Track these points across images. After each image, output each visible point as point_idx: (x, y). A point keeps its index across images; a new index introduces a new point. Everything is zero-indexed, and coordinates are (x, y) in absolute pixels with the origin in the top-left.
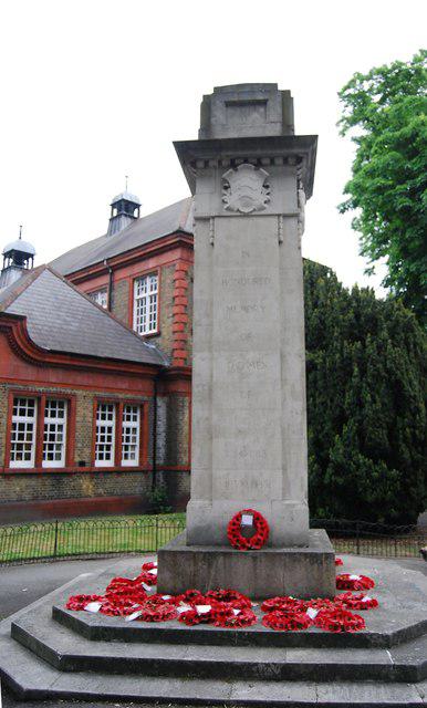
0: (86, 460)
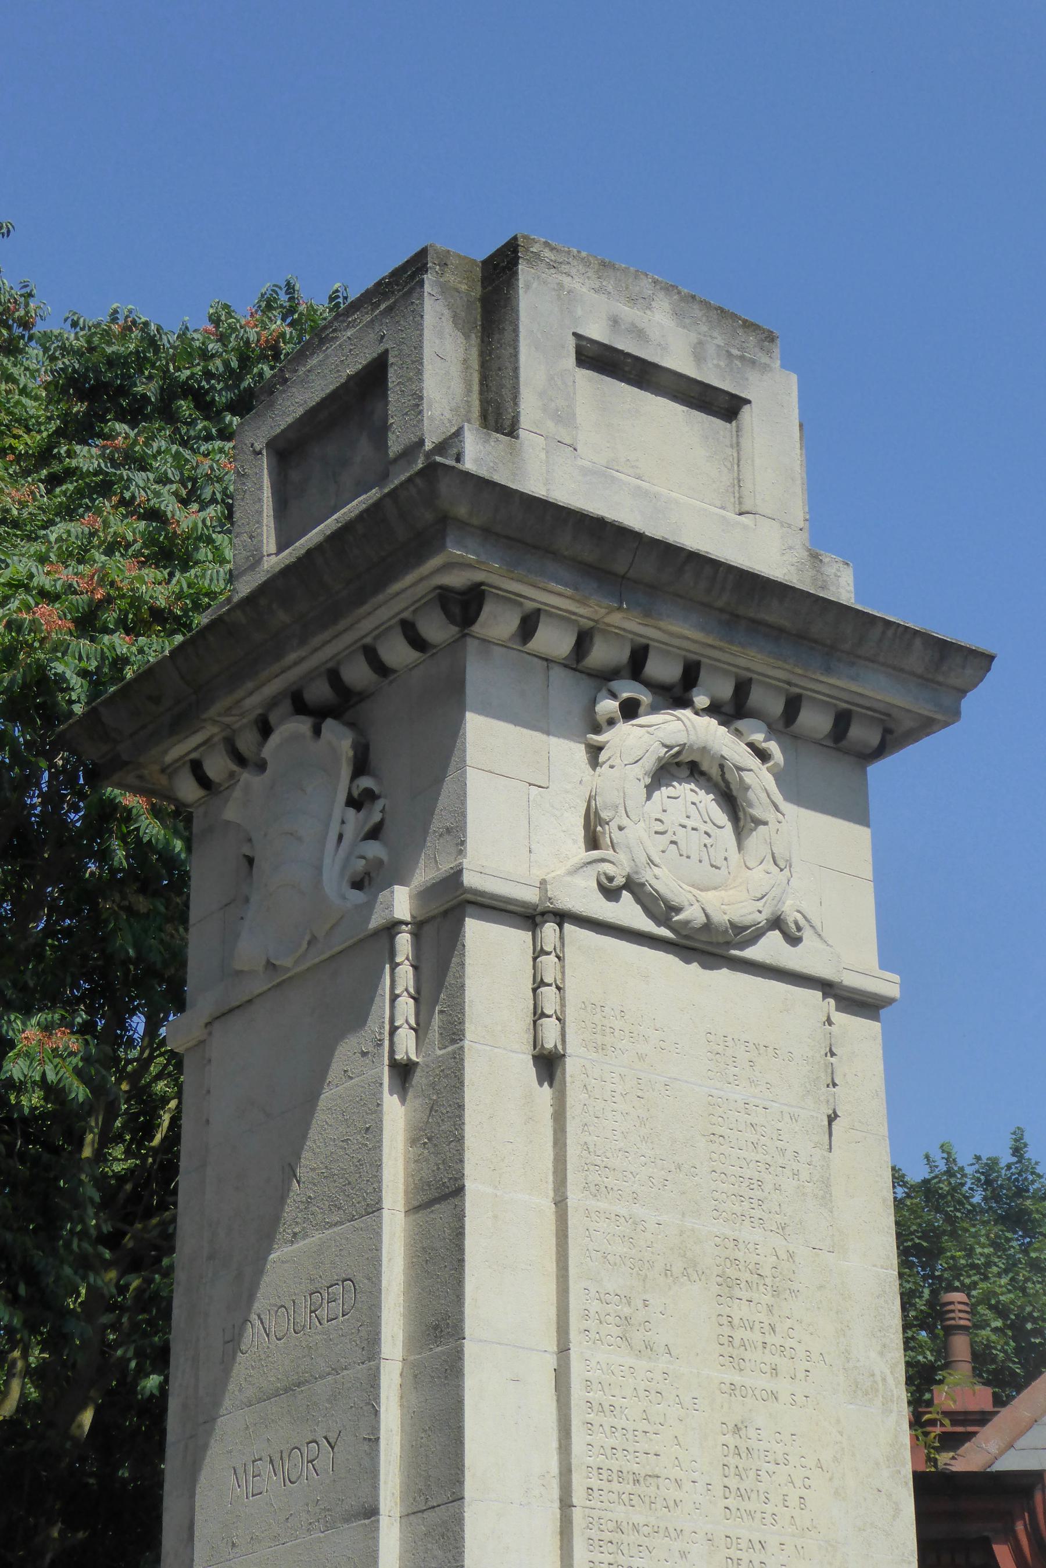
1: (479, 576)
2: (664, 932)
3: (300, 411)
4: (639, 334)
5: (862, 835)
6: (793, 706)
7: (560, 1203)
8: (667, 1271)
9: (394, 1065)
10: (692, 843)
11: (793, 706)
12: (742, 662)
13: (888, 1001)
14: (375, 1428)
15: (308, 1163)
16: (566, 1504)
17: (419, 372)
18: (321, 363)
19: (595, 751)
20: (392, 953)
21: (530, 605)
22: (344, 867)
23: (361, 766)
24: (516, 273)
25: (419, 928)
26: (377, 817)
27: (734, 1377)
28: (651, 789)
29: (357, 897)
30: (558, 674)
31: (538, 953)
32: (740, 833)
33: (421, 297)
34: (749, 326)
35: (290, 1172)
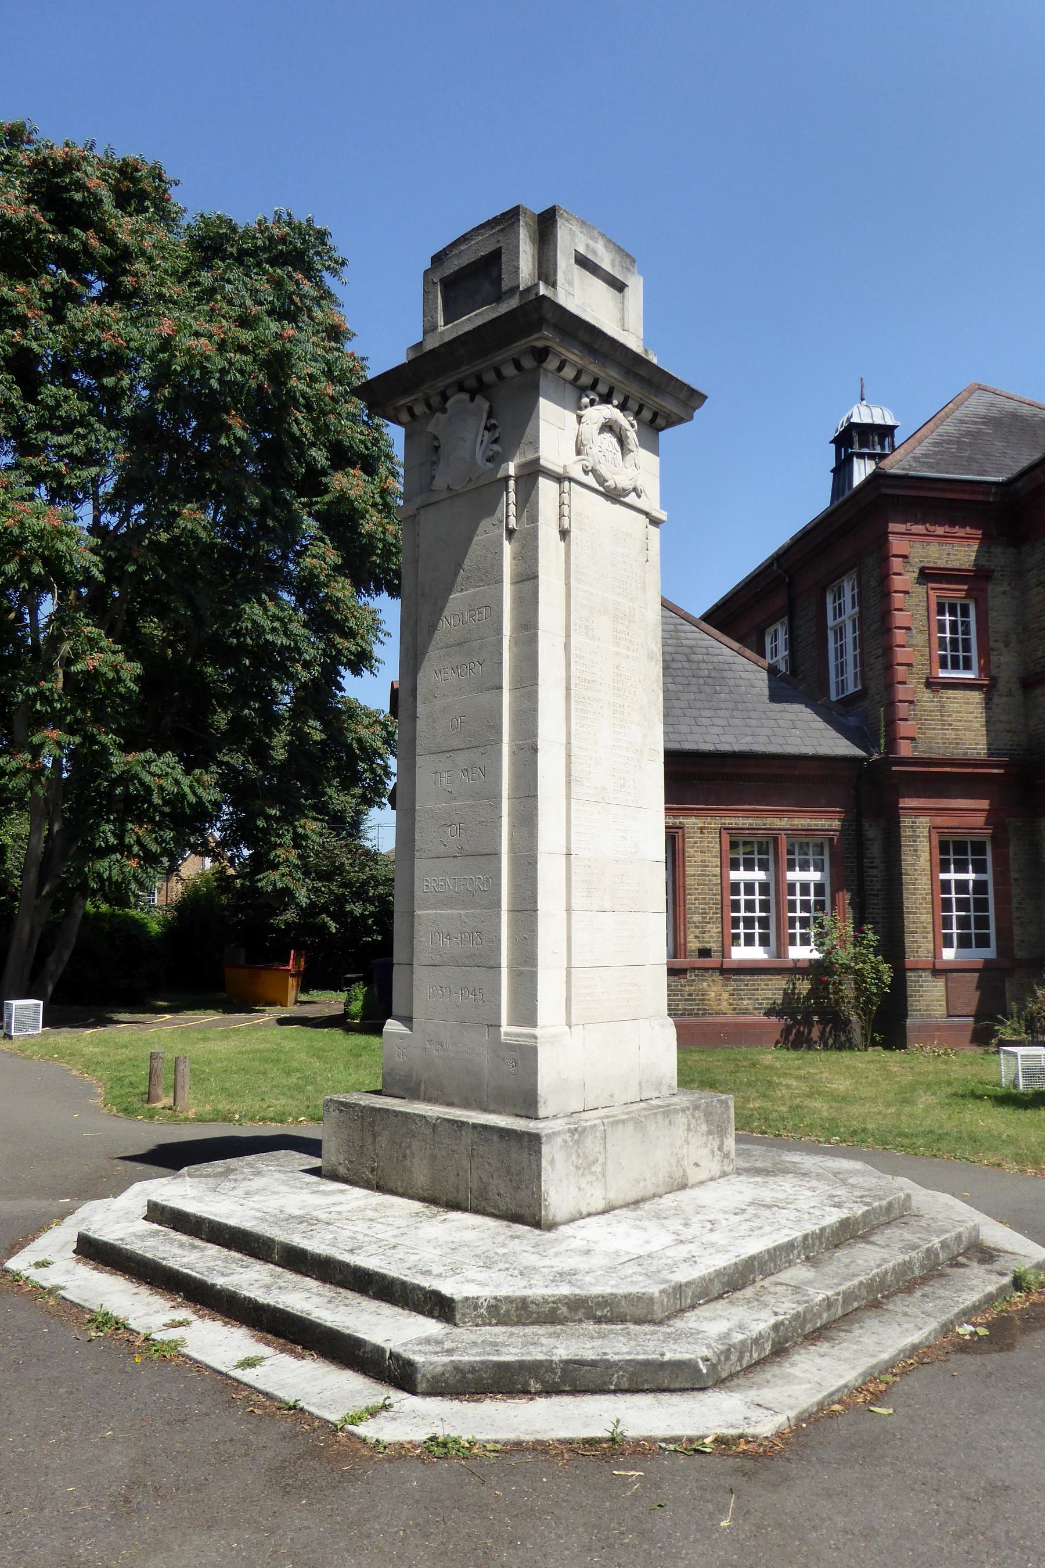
0: (714, 946)
1: (548, 343)
2: (601, 489)
3: (457, 268)
4: (595, 252)
5: (657, 459)
6: (641, 408)
7: (568, 585)
8: (599, 611)
9: (507, 529)
10: (610, 456)
11: (641, 408)
12: (628, 389)
13: (663, 522)
14: (501, 659)
15: (467, 563)
16: (568, 689)
17: (518, 258)
18: (467, 249)
19: (580, 418)
20: (507, 488)
21: (563, 357)
22: (484, 453)
23: (490, 415)
24: (556, 221)
25: (517, 479)
26: (497, 435)
27: (617, 649)
28: (599, 433)
29: (490, 465)
30: (568, 385)
31: (561, 492)
32: (623, 455)
33: (519, 227)
34: (628, 255)
35: (459, 566)
